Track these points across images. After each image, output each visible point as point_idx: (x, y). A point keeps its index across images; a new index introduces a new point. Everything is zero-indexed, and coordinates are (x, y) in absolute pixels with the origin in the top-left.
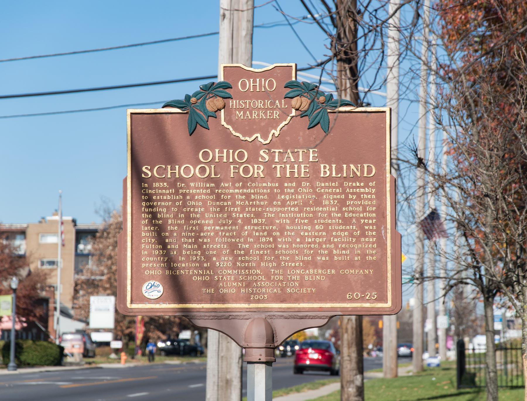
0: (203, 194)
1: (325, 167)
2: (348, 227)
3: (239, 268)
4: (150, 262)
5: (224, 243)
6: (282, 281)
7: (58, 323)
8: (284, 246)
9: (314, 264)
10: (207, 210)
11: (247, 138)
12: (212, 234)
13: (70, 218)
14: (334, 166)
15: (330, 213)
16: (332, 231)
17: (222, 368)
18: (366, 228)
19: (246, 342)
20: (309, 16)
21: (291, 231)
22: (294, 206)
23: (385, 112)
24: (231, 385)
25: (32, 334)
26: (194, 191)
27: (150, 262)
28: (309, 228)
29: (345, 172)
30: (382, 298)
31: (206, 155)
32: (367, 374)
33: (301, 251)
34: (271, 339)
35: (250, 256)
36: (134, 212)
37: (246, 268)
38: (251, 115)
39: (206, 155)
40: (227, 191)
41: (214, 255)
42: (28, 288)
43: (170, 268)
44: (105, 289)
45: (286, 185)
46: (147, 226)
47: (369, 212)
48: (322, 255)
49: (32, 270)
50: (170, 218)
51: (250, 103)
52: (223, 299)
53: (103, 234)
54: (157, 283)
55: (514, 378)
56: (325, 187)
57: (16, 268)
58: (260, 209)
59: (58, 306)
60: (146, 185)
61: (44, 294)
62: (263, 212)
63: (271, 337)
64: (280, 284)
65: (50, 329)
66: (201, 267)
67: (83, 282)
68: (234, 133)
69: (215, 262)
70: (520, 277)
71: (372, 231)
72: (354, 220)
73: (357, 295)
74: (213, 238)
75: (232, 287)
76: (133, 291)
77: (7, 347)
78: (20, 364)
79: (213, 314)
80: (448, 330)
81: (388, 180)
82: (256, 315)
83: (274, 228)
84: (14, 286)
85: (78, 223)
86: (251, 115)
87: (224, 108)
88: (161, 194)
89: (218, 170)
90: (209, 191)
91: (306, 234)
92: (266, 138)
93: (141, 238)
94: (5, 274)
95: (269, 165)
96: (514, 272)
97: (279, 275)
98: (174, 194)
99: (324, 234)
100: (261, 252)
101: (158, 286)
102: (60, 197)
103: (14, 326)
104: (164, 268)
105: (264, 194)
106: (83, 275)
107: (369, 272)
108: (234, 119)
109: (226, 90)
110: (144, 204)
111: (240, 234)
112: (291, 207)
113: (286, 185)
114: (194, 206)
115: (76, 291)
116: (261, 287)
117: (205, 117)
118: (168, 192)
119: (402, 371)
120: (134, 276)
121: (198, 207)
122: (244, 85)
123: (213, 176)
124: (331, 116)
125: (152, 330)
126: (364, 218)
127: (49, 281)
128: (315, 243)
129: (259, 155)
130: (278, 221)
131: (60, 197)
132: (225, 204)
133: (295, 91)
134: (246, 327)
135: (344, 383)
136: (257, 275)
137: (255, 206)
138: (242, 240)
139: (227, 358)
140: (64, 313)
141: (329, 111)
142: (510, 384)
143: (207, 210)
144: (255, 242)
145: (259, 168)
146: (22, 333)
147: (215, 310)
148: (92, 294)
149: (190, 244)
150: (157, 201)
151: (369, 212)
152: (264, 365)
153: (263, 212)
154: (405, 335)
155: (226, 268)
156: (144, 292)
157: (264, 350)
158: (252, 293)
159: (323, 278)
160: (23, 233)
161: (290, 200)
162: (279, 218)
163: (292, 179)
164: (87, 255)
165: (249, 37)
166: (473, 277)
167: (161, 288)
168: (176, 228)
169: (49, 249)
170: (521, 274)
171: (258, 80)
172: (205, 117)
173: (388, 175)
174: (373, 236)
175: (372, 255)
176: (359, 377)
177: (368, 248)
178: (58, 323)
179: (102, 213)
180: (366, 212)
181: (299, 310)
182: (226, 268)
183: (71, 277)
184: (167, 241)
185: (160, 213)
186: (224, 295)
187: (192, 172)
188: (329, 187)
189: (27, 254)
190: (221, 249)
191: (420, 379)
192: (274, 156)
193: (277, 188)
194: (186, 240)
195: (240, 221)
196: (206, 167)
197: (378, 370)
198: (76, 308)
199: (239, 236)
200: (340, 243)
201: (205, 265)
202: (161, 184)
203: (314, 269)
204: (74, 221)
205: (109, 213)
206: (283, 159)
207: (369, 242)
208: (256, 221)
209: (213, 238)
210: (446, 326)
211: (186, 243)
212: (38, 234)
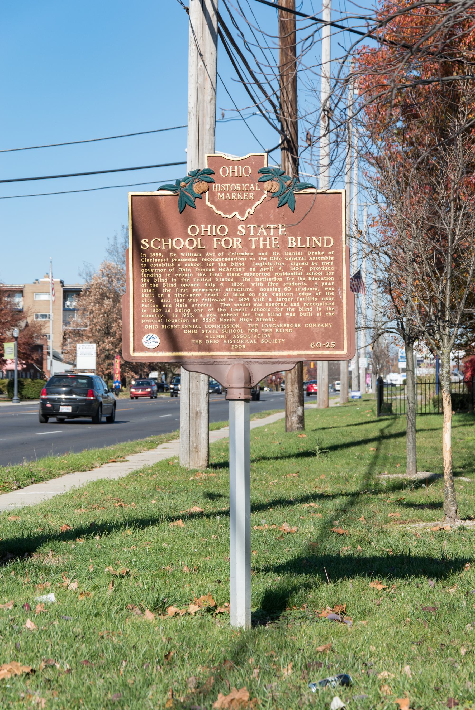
0: (191, 262)
1: (292, 239)
2: (311, 289)
3: (221, 323)
4: (148, 318)
5: (209, 303)
6: (257, 334)
7: (51, 365)
8: (259, 305)
9: (283, 319)
10: (195, 276)
11: (228, 216)
12: (199, 295)
13: (59, 280)
14: (299, 238)
15: (296, 277)
16: (298, 292)
17: (192, 402)
18: (326, 289)
19: (227, 383)
20: (258, 112)
21: (265, 292)
22: (267, 271)
23: (341, 193)
24: (200, 416)
25: (30, 374)
26: (184, 260)
27: (148, 318)
28: (279, 290)
29: (308, 243)
30: (339, 347)
31: (193, 229)
32: (306, 405)
33: (272, 309)
34: (249, 381)
35: (231, 313)
36: (135, 277)
37: (227, 323)
38: (231, 197)
39: (193, 229)
40: (211, 259)
41: (201, 313)
42: (27, 337)
43: (165, 323)
44: (88, 338)
45: (260, 254)
46: (146, 288)
47: (329, 276)
48: (290, 312)
49: (29, 322)
50: (164, 282)
51: (229, 186)
52: (209, 348)
53: (86, 292)
54: (155, 335)
55: (423, 407)
56: (292, 256)
57: (17, 321)
58: (238, 274)
59: (51, 351)
60: (145, 255)
61: (39, 342)
62: (241, 276)
63: (249, 379)
64: (255, 336)
65: (44, 370)
66: (191, 323)
67: (70, 332)
68: (217, 211)
69: (202, 318)
70: (441, 327)
71: (331, 291)
72: (316, 283)
73: (319, 345)
74: (200, 299)
75: (216, 339)
76: (136, 342)
77: (11, 384)
78: (22, 398)
79: (201, 360)
80: (367, 369)
81: (344, 249)
82: (236, 362)
83: (250, 290)
84: (16, 335)
85: (65, 284)
86: (231, 197)
87: (208, 190)
88: (157, 262)
89: (204, 242)
90: (196, 260)
91: (277, 294)
92: (243, 216)
93: (141, 299)
94: (8, 325)
95: (245, 238)
96: (436, 323)
97: (255, 328)
98: (167, 262)
99: (292, 294)
100: (240, 310)
101: (156, 338)
102: (51, 262)
103: (16, 367)
104: (160, 324)
105: (241, 262)
106: (70, 327)
107: (329, 325)
108: (216, 200)
109: (210, 176)
110: (143, 270)
111: (222, 295)
112: (264, 272)
113: (260, 254)
114: (184, 273)
115: (65, 339)
116: (240, 339)
117: (193, 199)
118: (162, 260)
119: (332, 403)
120: (136, 329)
121: (188, 273)
122: (224, 172)
123: (199, 247)
124: (296, 197)
125: (127, 371)
126: (324, 281)
127: (44, 331)
128: (284, 302)
129: (237, 230)
130: (253, 284)
131: (51, 262)
132: (210, 270)
133: (267, 176)
134: (228, 371)
135: (288, 413)
136: (236, 329)
137: (234, 272)
138: (224, 300)
139: (196, 395)
140: (56, 357)
141: (295, 192)
142: (419, 412)
143: (195, 276)
144: (234, 302)
145: (237, 240)
146: (22, 373)
147: (202, 358)
148: (77, 341)
149: (181, 303)
150: (154, 268)
151: (329, 276)
152: (243, 402)
153: (241, 276)
154: (334, 375)
155: (211, 323)
156: (144, 343)
157: (243, 389)
158: (232, 344)
159: (291, 331)
160: (21, 292)
161: (263, 267)
162: (254, 282)
163: (264, 249)
164: (73, 310)
165: (212, 130)
166: (397, 327)
167: (158, 340)
168: (170, 290)
169: (41, 305)
170: (441, 324)
171: (236, 167)
172: (193, 199)
173: (344, 246)
174: (332, 296)
175: (331, 312)
176: (300, 408)
177: (328, 306)
178: (51, 365)
179: (84, 275)
180: (326, 276)
181: (272, 357)
182: (211, 323)
183: (60, 328)
184: (162, 301)
185: (156, 278)
186: (210, 345)
187: (182, 244)
188: (295, 256)
189: (25, 310)
190: (207, 308)
191: (347, 408)
192: (250, 231)
193: (252, 257)
194: (178, 300)
195: (222, 284)
196: (194, 239)
197: (312, 402)
198: (65, 353)
199: (222, 297)
200: (304, 302)
201: (194, 321)
202: (157, 254)
203: (283, 323)
204: (62, 282)
205: (90, 276)
206: (257, 233)
207: (328, 301)
208: (235, 284)
209: (200, 299)
210: (366, 366)
211: (178, 303)
212: (33, 293)
